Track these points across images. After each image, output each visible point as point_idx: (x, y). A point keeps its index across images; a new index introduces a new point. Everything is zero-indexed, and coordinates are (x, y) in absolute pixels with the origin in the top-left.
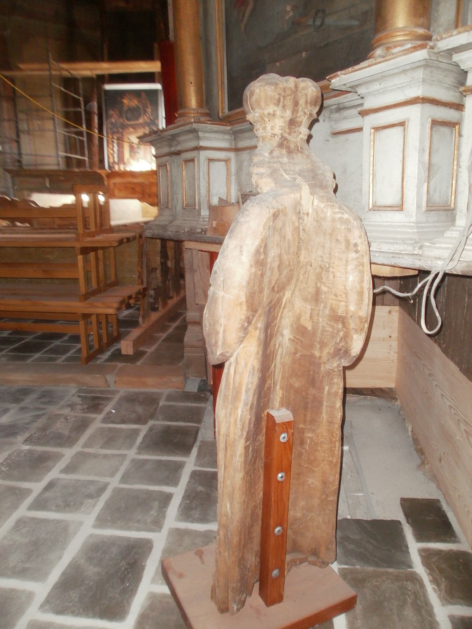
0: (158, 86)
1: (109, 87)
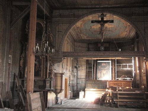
0: (110, 61)
1: (98, 61)
